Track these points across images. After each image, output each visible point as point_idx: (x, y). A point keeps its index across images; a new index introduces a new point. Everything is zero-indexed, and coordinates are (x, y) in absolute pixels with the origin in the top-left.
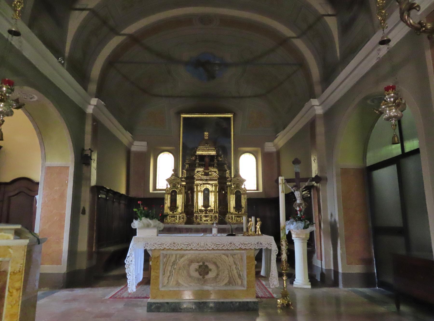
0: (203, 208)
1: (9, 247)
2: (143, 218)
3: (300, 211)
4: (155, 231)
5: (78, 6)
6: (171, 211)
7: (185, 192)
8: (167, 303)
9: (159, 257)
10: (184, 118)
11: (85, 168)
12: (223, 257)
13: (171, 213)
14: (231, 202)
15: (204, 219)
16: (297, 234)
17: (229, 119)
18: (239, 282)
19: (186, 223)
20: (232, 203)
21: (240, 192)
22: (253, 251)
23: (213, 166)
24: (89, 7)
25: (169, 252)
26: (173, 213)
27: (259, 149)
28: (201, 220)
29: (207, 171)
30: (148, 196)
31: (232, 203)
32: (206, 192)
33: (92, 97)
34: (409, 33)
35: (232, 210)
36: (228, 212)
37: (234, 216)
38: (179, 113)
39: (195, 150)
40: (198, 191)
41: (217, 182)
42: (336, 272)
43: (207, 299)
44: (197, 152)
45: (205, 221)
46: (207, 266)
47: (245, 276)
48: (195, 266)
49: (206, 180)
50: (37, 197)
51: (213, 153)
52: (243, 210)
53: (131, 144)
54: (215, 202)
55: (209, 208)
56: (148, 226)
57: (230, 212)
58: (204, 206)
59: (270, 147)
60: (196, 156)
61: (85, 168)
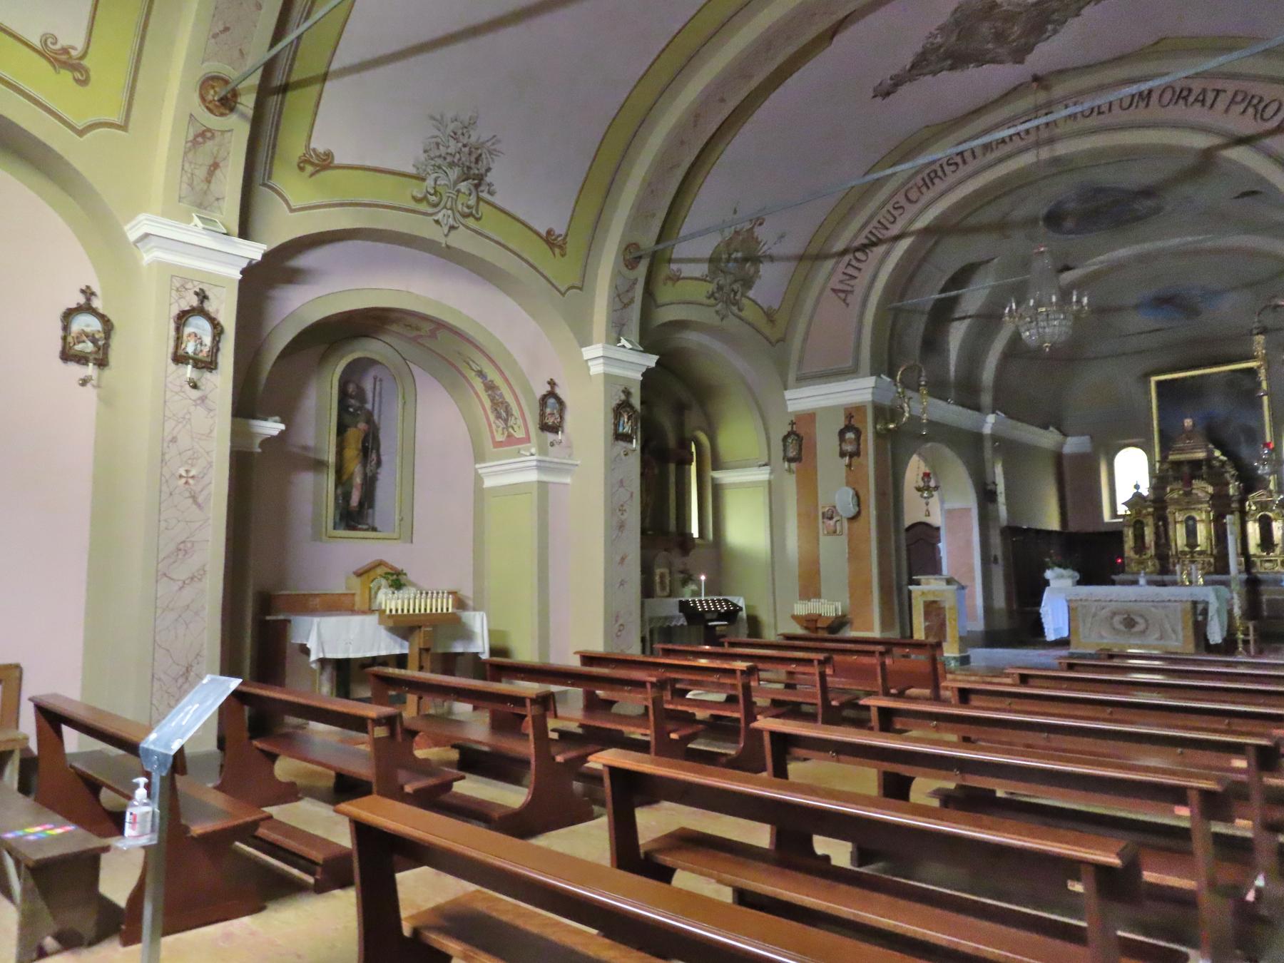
0: (1187, 549)
5: (957, 316)
6: (1263, 551)
10: (1159, 384)
11: (991, 506)
12: (1153, 609)
13: (1137, 557)
18: (1174, 636)
26: (1140, 556)
30: (1103, 529)
33: (987, 414)
38: (1147, 376)
46: (1132, 620)
48: (1117, 619)
50: (940, 545)
53: (1062, 445)
54: (1209, 538)
55: (1198, 549)
56: (1062, 577)
58: (1187, 545)
61: (991, 506)
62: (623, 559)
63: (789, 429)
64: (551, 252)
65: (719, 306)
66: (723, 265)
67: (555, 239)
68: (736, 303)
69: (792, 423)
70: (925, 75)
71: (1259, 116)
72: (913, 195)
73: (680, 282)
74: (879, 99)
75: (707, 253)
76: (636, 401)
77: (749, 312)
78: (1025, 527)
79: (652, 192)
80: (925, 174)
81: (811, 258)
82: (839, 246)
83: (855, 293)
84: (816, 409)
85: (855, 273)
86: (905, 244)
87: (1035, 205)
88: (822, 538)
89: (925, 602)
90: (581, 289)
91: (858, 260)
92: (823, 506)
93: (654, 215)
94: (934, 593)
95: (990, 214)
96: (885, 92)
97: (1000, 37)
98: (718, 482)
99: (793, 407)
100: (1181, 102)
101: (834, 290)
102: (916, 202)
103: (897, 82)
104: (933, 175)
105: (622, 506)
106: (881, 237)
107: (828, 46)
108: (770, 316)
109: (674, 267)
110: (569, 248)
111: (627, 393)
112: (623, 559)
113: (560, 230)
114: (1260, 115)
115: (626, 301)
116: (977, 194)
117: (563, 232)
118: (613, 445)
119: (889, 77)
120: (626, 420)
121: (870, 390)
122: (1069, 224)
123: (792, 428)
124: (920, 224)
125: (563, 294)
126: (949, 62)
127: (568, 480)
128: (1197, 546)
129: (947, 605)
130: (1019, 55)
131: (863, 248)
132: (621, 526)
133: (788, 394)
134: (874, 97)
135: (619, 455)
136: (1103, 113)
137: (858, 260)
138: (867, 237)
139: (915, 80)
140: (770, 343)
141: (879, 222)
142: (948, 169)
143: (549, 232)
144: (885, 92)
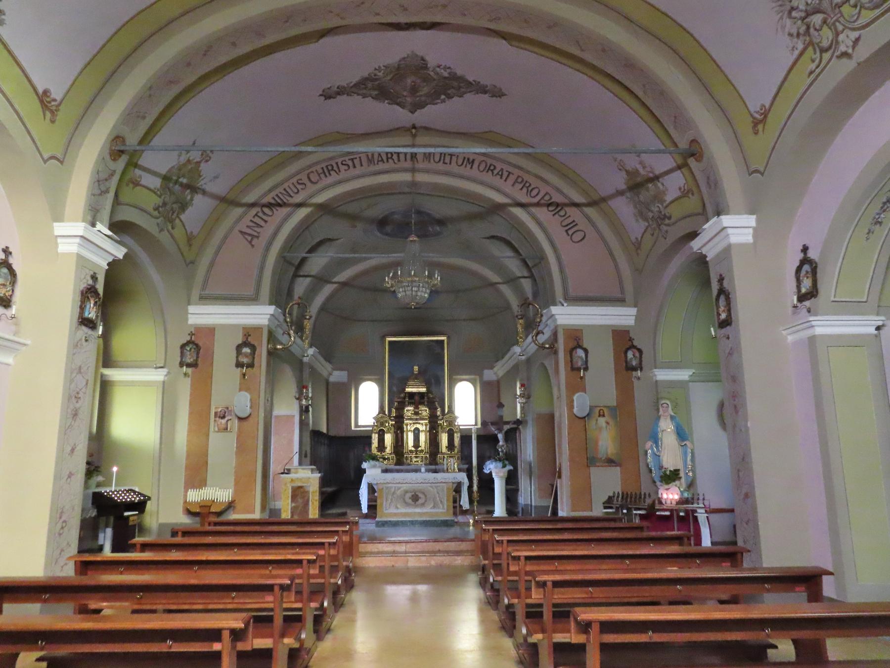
0: (413, 449)
1: (309, 478)
2: (371, 461)
3: (502, 451)
4: (379, 470)
5: (301, 274)
6: (378, 451)
7: (394, 432)
8: (390, 521)
9: (382, 489)
10: (390, 342)
13: (379, 453)
14: (443, 441)
15: (415, 460)
16: (496, 473)
17: (443, 341)
19: (396, 464)
20: (444, 439)
21: (452, 430)
22: (451, 484)
23: (422, 403)
24: (313, 273)
25: (390, 485)
26: (381, 453)
27: (477, 377)
28: (411, 461)
29: (417, 410)
30: (349, 434)
31: (444, 439)
32: (417, 432)
34: (537, 350)
35: (444, 450)
36: (439, 452)
37: (446, 456)
39: (405, 385)
40: (408, 431)
41: (427, 421)
42: (531, 506)
43: (429, 77)
44: (407, 389)
45: (415, 462)
46: (417, 495)
47: (446, 502)
48: (409, 495)
49: (416, 419)
51: (423, 390)
52: (456, 450)
54: (426, 442)
55: (420, 449)
56: (374, 467)
57: (441, 452)
59: (489, 375)
60: (406, 393)
62: (73, 450)
63: (188, 338)
64: (42, 114)
65: (159, 221)
66: (171, 185)
67: (49, 102)
68: (172, 221)
69: (191, 334)
70: (358, 95)
71: (529, 193)
72: (314, 177)
73: (138, 188)
74: (323, 98)
75: (163, 171)
76: (100, 288)
77: (178, 232)
78: (749, 425)
79: (150, 96)
80: (324, 165)
81: (228, 201)
82: (250, 198)
83: (260, 238)
84: (216, 325)
85: (262, 223)
86: (303, 212)
87: (379, 210)
88: (212, 435)
89: (293, 488)
90: (62, 162)
91: (264, 213)
92: (217, 404)
93: (144, 118)
94: (301, 480)
95: (352, 208)
96: (327, 95)
97: (414, 90)
98: (107, 379)
99: (193, 320)
100: (490, 172)
101: (241, 232)
102: (316, 183)
103: (341, 91)
104: (330, 168)
105: (78, 393)
106: (285, 200)
107: (315, 42)
108: (190, 239)
109: (138, 172)
110: (60, 116)
111: (94, 278)
112: (73, 450)
113: (57, 94)
114: (529, 192)
115: (103, 189)
116: (361, 190)
117: (59, 98)
118: (77, 329)
119: (338, 84)
120: (92, 305)
121: (268, 316)
122: (388, 229)
123: (191, 338)
124: (320, 199)
125: (45, 161)
126: (376, 92)
127: (10, 360)
128: (420, 447)
129: (311, 490)
130: (416, 107)
131: (269, 205)
132: (75, 415)
133: (191, 309)
134: (321, 95)
135: (81, 340)
136: (446, 163)
137: (264, 213)
138: (273, 198)
139: (351, 95)
140: (185, 261)
141: (285, 190)
142: (342, 168)
143: (46, 92)
144: (327, 95)
